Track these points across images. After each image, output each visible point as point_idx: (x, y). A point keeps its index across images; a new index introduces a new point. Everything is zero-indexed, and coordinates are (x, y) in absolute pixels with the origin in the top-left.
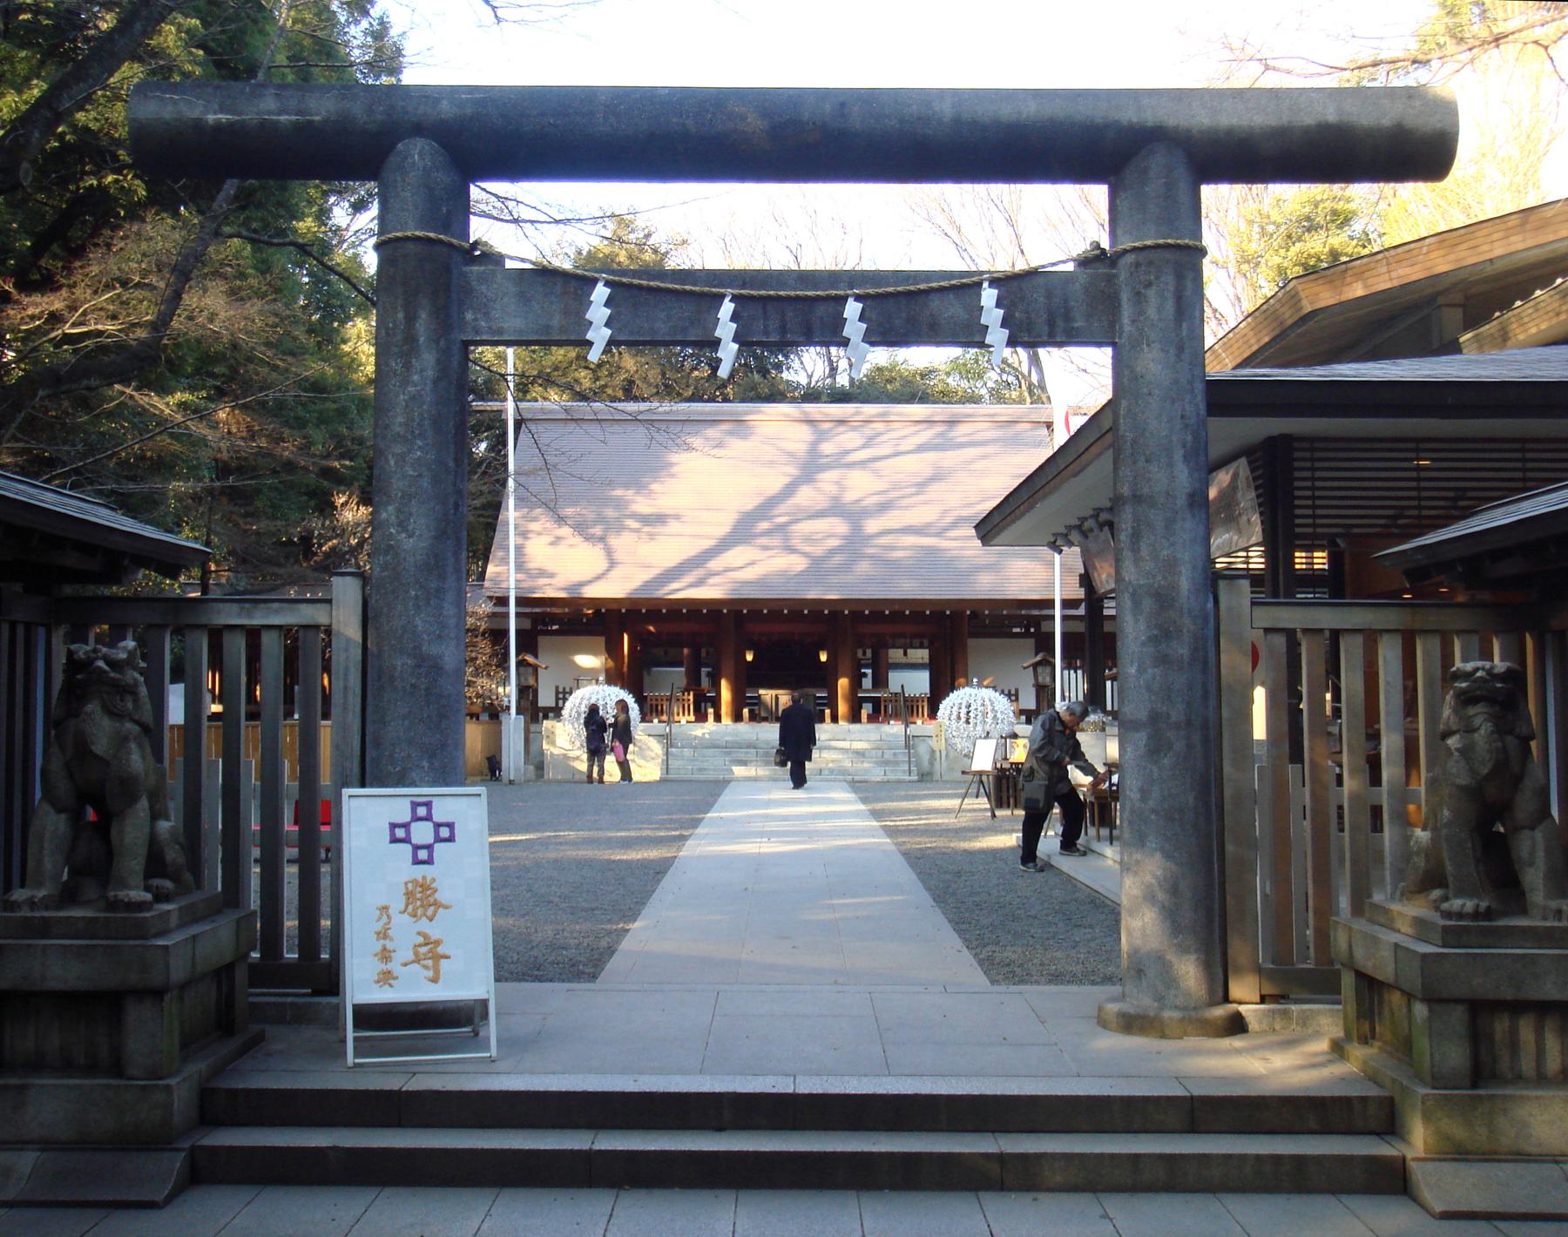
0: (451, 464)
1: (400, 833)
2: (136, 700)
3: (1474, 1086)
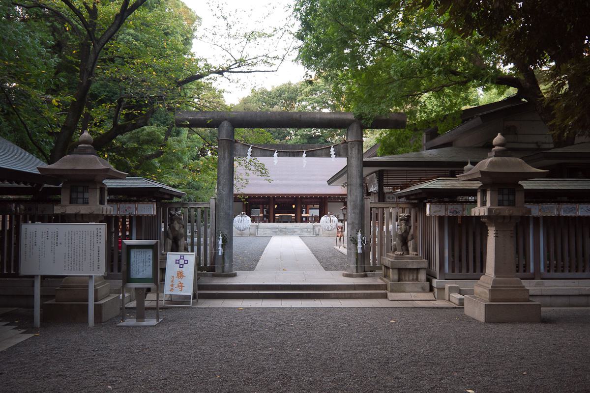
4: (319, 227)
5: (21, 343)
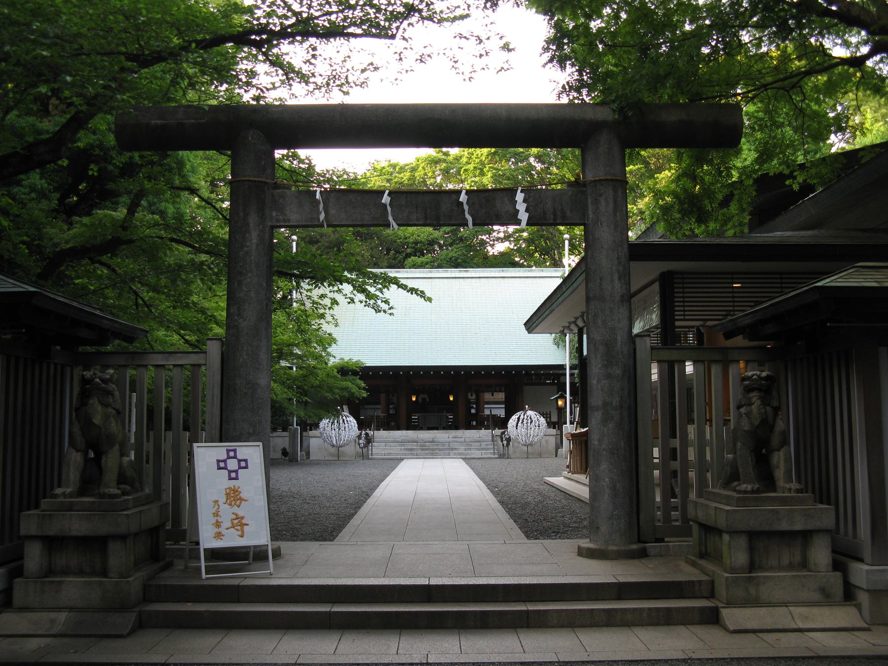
0: (265, 285)
3: (750, 572)
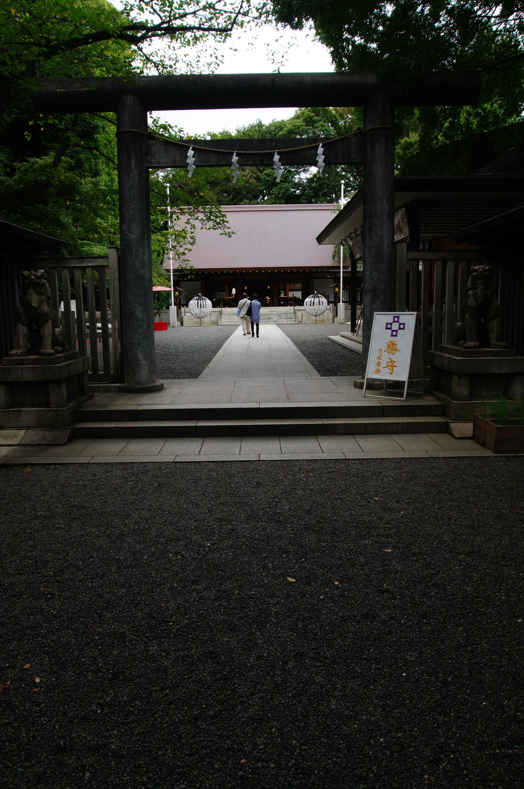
0: (145, 209)
1: (389, 326)
2: (45, 289)
4: (302, 312)
5: (239, 465)
